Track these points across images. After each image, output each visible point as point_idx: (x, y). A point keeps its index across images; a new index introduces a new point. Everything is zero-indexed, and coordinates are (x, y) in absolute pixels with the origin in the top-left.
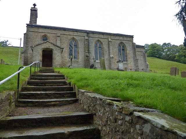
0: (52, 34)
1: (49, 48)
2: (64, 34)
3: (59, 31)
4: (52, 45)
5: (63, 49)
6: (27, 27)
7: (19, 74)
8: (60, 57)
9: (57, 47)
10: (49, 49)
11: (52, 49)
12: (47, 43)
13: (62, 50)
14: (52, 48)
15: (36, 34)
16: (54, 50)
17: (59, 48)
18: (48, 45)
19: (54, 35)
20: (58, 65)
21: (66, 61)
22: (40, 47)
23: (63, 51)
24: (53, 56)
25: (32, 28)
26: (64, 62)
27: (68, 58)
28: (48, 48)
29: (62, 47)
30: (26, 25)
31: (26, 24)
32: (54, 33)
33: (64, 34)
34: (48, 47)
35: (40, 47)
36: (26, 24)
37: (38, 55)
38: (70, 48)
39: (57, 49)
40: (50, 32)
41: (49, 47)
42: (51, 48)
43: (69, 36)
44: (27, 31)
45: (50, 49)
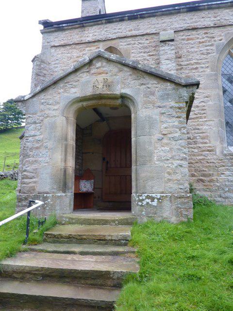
0: (136, 41)
1: (106, 91)
2: (194, 29)
3: (167, 20)
4: (127, 72)
5: (197, 85)
6: (43, 32)
7: (29, 213)
8: (175, 145)
9: (152, 83)
10: (108, 102)
11: (123, 97)
12: (99, 64)
13: (185, 93)
14: (127, 91)
15: (75, 55)
16: (139, 99)
17: (169, 86)
18: (100, 78)
19: (144, 41)
20: (166, 203)
21: (210, 157)
22: (57, 98)
23: (192, 99)
24: (133, 139)
25: (60, 33)
26: (200, 161)
27: (222, 141)
28: (100, 97)
29: (184, 76)
30: (42, 27)
31: (40, 22)
32: (148, 31)
33: (194, 29)
34: (101, 90)
35: (57, 98)
36: (40, 22)
37: (50, 144)
38: (225, 91)
39: (153, 94)
40: (129, 34)
41: (108, 86)
42: (119, 90)
43: (217, 32)
44: (44, 47)
45: (114, 98)
